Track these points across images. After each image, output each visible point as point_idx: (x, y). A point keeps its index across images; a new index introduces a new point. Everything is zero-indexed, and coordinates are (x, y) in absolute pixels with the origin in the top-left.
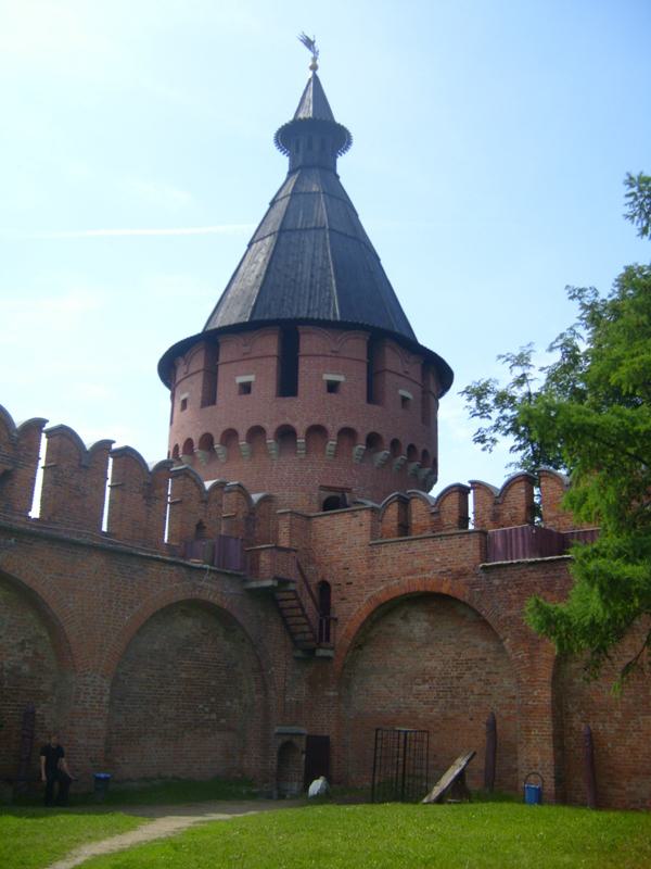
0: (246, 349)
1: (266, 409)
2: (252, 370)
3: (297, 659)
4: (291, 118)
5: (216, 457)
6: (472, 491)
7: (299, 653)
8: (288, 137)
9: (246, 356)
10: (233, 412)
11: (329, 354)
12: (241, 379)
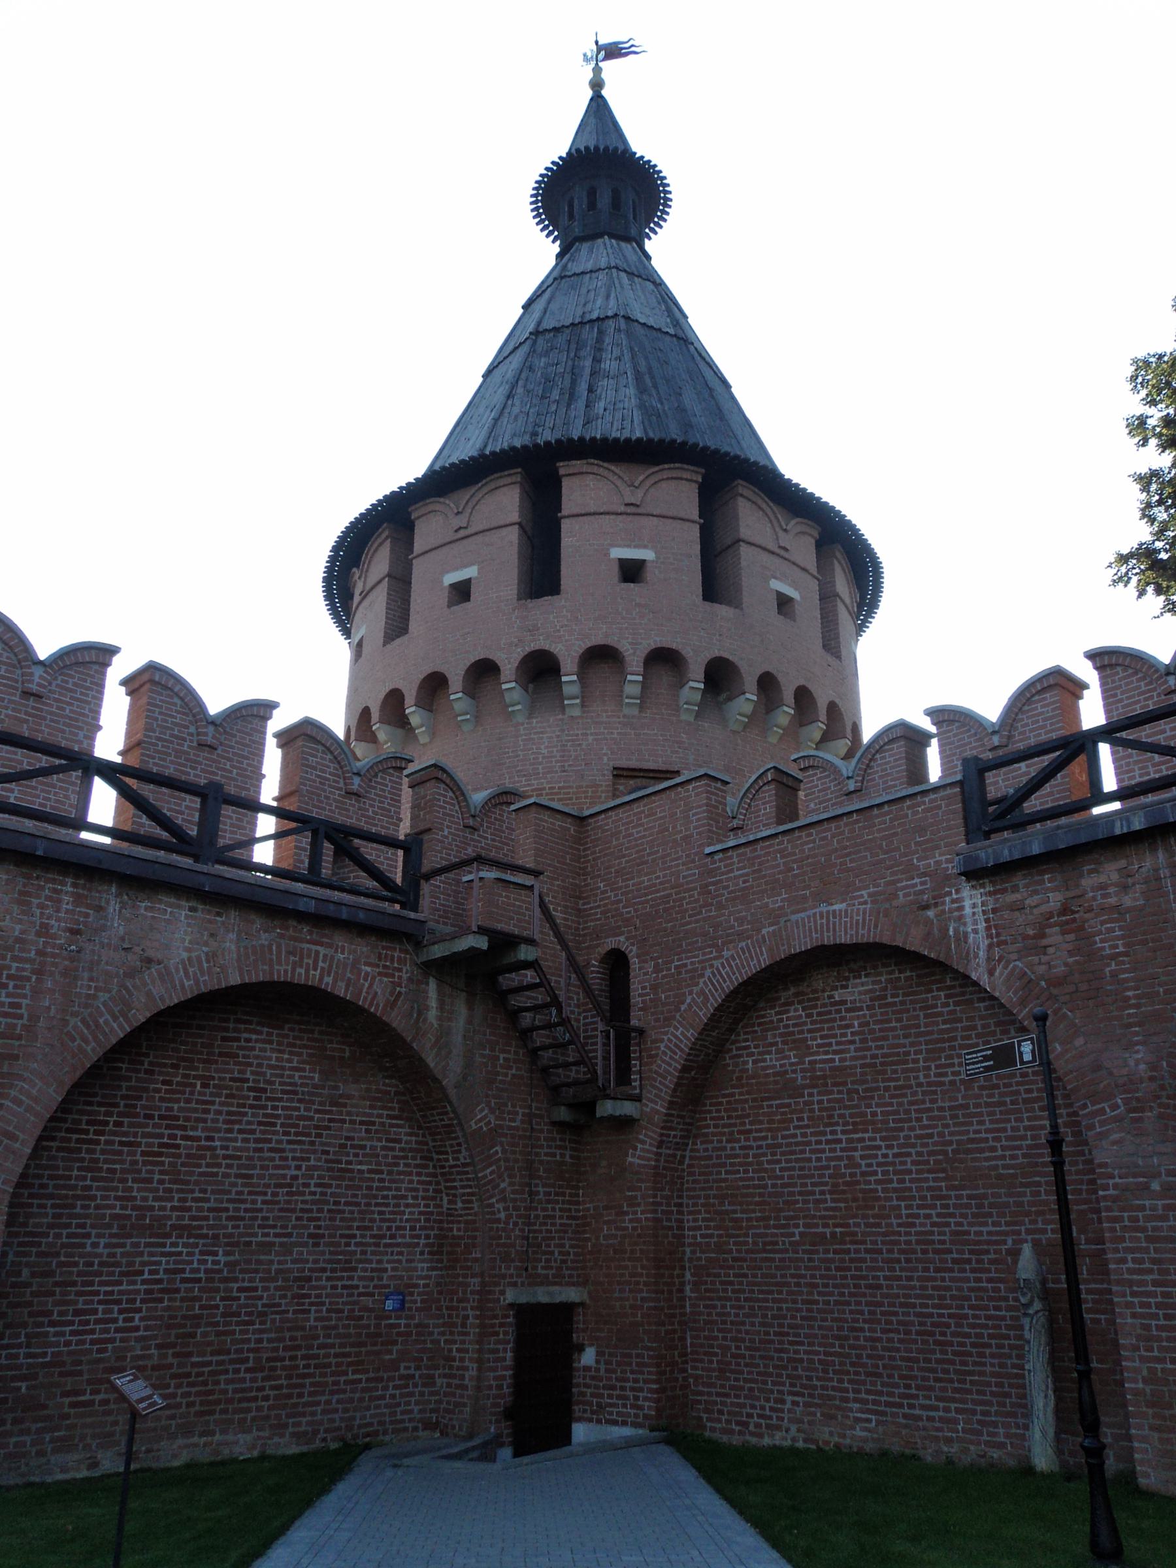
0: (461, 521)
1: (504, 627)
2: (480, 547)
3: (560, 1125)
5: (416, 737)
6: (934, 742)
7: (563, 1114)
9: (462, 533)
10: (441, 641)
11: (622, 509)
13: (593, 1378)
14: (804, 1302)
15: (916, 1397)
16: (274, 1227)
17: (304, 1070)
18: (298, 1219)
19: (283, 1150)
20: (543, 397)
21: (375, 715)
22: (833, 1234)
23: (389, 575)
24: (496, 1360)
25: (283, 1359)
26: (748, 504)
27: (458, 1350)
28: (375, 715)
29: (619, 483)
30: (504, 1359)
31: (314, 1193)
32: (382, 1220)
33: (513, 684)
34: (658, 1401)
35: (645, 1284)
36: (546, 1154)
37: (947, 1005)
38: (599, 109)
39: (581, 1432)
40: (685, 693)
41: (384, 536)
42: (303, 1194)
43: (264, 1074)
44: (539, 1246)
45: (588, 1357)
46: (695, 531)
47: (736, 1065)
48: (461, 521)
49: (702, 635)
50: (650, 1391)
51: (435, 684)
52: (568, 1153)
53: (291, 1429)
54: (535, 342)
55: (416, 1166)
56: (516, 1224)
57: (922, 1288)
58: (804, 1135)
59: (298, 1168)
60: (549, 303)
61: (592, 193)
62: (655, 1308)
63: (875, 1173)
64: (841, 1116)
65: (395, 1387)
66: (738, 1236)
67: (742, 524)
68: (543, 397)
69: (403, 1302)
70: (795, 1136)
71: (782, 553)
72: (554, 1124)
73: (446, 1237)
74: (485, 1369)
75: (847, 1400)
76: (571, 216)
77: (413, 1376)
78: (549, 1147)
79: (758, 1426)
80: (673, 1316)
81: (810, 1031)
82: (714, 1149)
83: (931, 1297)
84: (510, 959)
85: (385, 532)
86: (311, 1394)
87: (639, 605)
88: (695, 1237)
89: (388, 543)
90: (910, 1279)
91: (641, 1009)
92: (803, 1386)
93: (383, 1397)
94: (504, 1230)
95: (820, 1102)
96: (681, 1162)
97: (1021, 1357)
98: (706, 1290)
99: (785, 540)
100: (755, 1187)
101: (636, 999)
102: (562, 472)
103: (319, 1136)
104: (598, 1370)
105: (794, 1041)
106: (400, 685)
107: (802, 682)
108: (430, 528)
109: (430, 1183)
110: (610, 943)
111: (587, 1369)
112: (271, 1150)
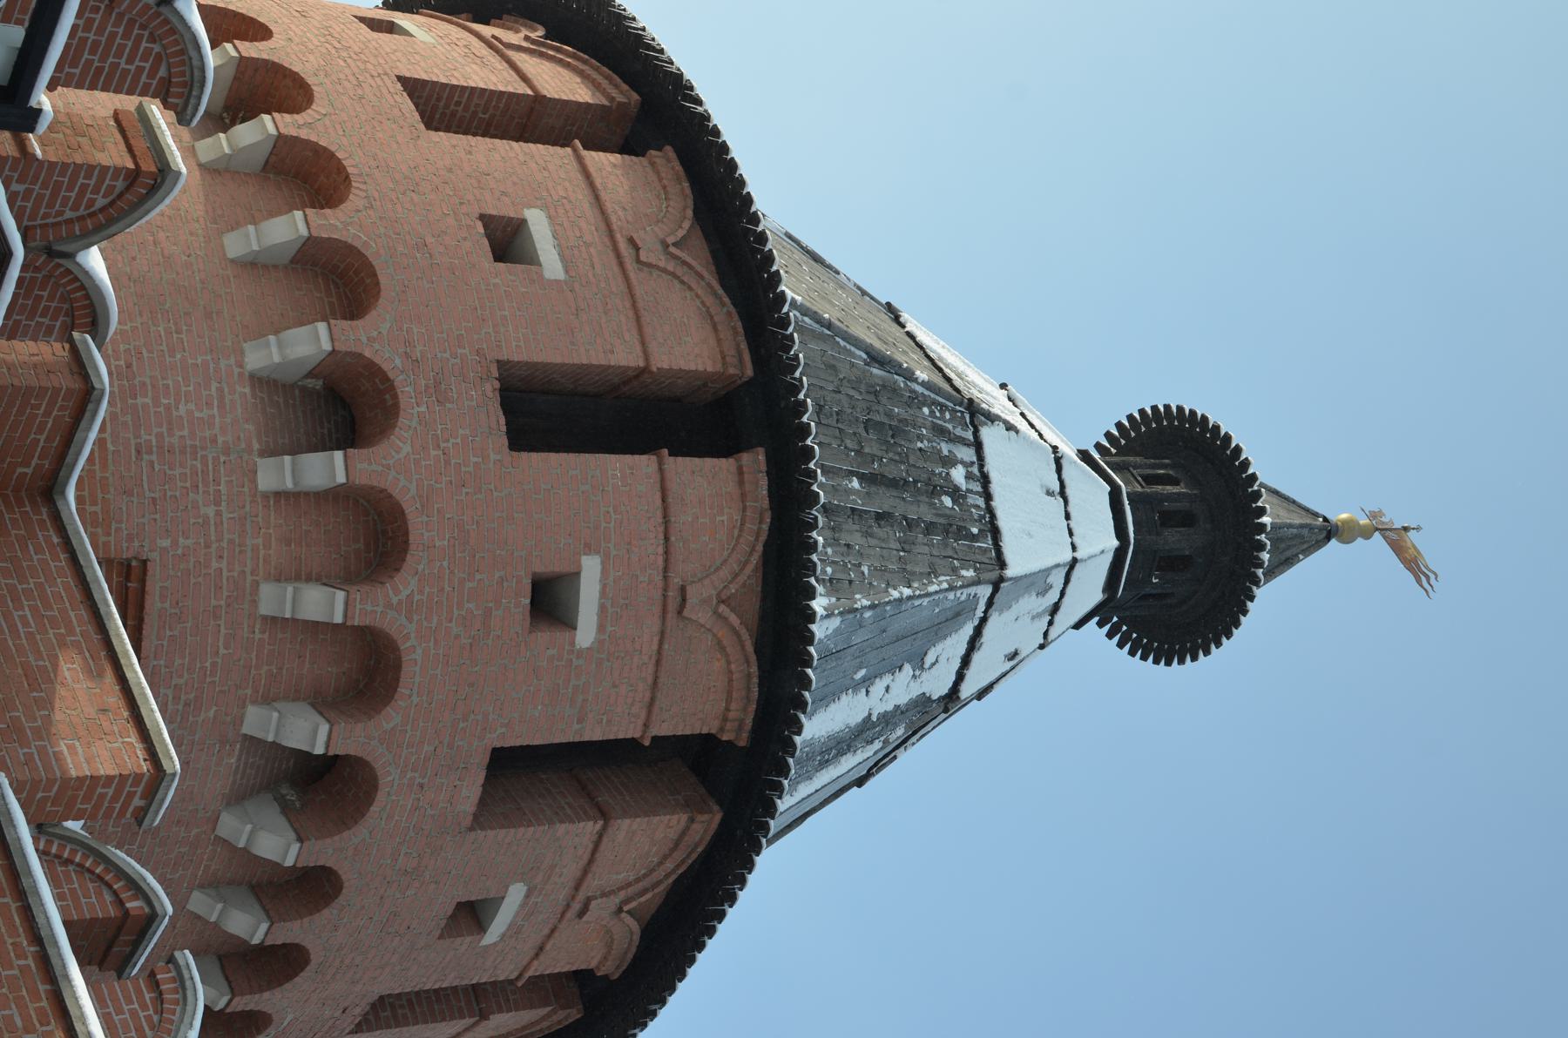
1: (440, 340)
4: (1262, 478)
11: (676, 581)
12: (538, 224)
21: (251, 49)
26: (673, 834)
28: (251, 49)
29: (725, 573)
41: (614, 93)
46: (625, 728)
49: (423, 755)
61: (1186, 520)
67: (639, 823)
71: (576, 906)
85: (624, 95)
87: (488, 613)
99: (601, 910)
102: (746, 457)
106: (319, 106)
107: (316, 958)
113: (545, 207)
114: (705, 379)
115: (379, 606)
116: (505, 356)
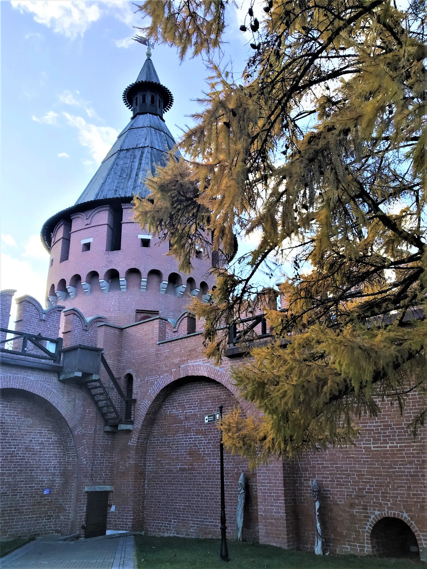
0: (88, 222)
1: (101, 260)
2: (93, 231)
3: (107, 432)
7: (108, 429)
8: (132, 95)
13: (114, 515)
14: (179, 490)
15: (208, 519)
16: (6, 468)
17: (18, 416)
18: (14, 465)
19: (10, 442)
20: (120, 176)
22: (188, 468)
23: (63, 238)
24: (80, 510)
25: (7, 510)
27: (68, 507)
30: (83, 510)
31: (20, 456)
32: (44, 465)
33: (103, 280)
34: (132, 522)
35: (131, 484)
36: (102, 442)
37: (224, 396)
38: (149, 65)
39: (108, 532)
40: (162, 285)
42: (17, 456)
43: (4, 418)
44: (98, 472)
45: (113, 509)
47: (164, 413)
48: (88, 222)
50: (130, 519)
51: (77, 278)
52: (110, 441)
53: (9, 533)
54: (119, 154)
55: (58, 447)
56: (90, 465)
57: (212, 485)
58: (182, 436)
59: (15, 448)
60: (125, 138)
62: (134, 492)
63: (201, 448)
64: (193, 430)
65: (46, 519)
66: (161, 468)
68: (120, 176)
69: (50, 492)
70: (180, 436)
72: (105, 432)
73: (66, 470)
74: (75, 512)
75: (189, 520)
76: (136, 105)
77: (52, 516)
78: (103, 440)
79: (163, 529)
80: (140, 495)
81: (186, 402)
82: (156, 440)
83: (214, 488)
84: (90, 379)
86: (16, 522)
88: (149, 469)
89: (63, 226)
90: (209, 482)
91: (135, 394)
92: (177, 516)
93: (42, 523)
94: (85, 467)
95: (187, 425)
96: (146, 444)
97: (236, 506)
98: (152, 486)
100: (167, 452)
101: (134, 391)
103: (22, 437)
104: (115, 513)
105: (181, 406)
108: (78, 223)
109: (61, 452)
110: (128, 372)
111: (112, 512)
112: (6, 442)
113: (81, 240)
114: (110, 212)
115: (144, 273)
116: (104, 248)
